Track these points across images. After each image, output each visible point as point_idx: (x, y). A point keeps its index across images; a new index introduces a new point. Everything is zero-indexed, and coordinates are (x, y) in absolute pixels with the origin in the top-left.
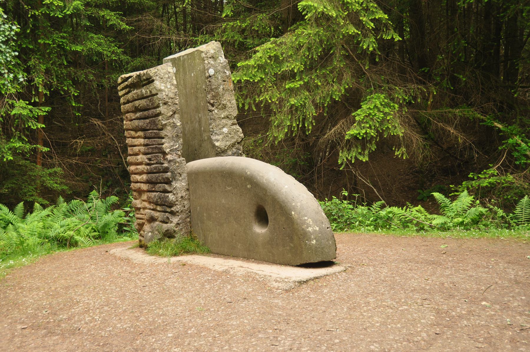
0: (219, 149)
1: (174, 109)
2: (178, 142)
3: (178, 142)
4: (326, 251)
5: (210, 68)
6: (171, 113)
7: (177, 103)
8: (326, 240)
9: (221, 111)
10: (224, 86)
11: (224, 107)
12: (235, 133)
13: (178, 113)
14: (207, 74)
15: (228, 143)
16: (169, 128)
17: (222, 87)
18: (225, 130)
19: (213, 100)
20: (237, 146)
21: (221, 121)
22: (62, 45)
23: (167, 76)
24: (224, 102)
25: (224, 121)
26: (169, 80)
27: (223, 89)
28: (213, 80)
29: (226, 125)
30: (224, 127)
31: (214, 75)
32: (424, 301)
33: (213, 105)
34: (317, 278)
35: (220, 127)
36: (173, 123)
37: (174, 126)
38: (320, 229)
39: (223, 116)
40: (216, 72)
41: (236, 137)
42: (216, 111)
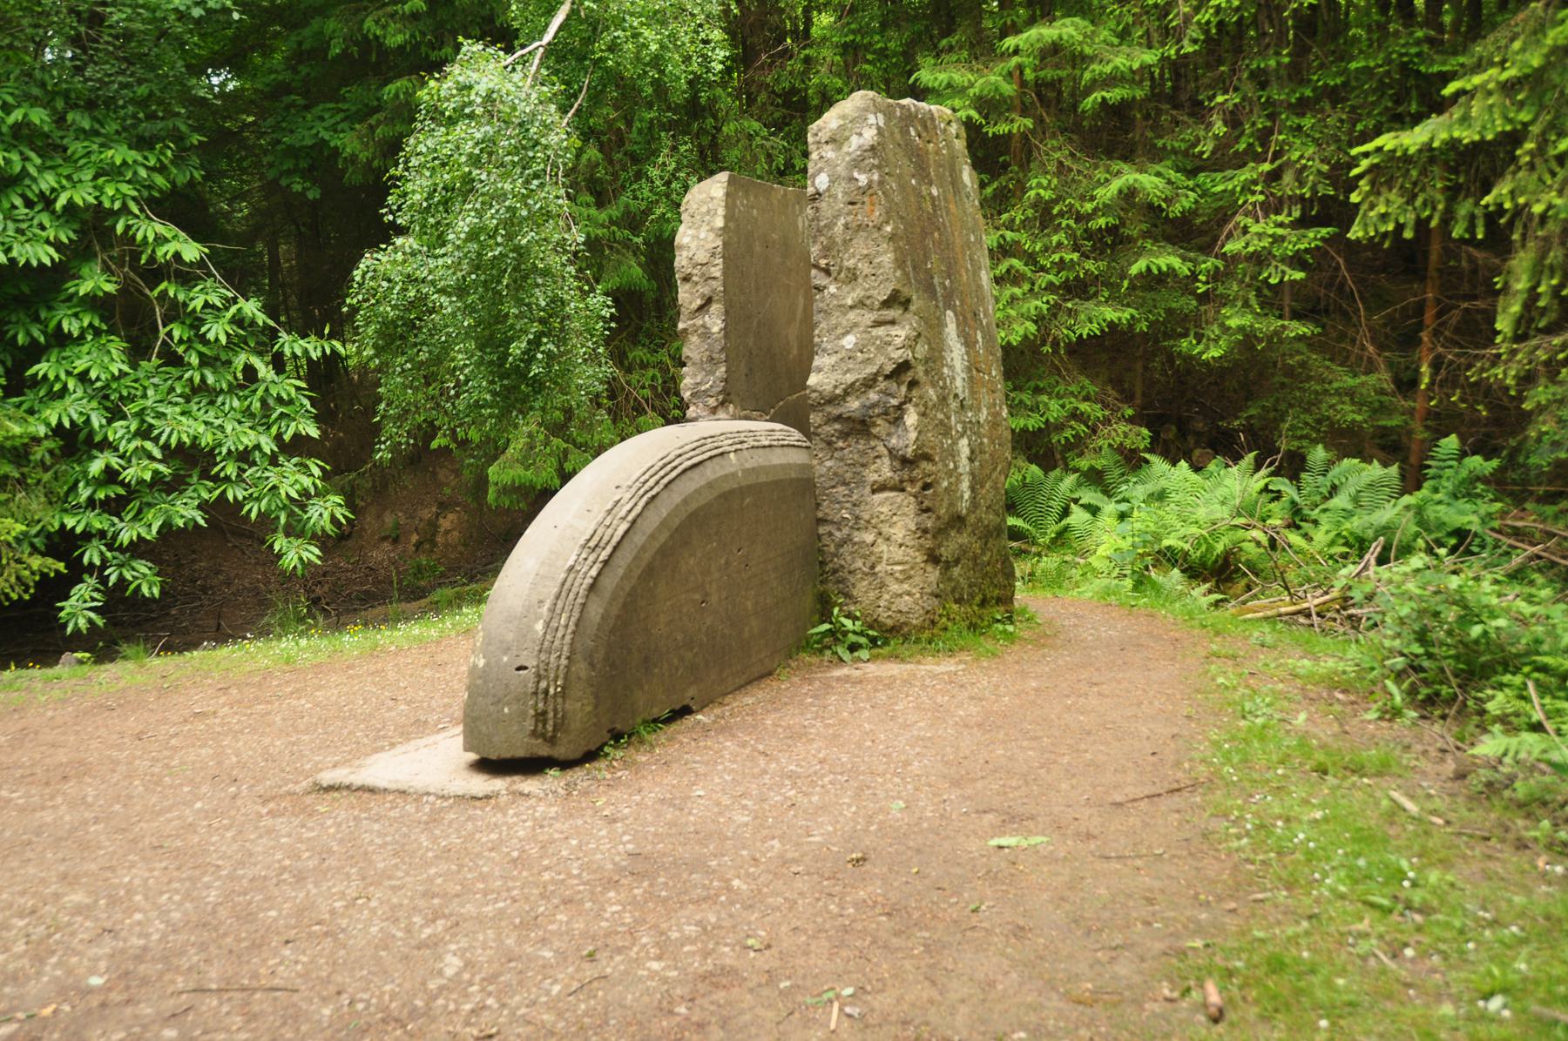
0: (814, 395)
1: (706, 290)
2: (713, 373)
3: (713, 373)
4: (484, 729)
5: (820, 170)
6: (699, 302)
7: (718, 274)
8: (490, 700)
9: (846, 289)
10: (849, 219)
11: (853, 277)
12: (878, 348)
13: (718, 301)
14: (810, 190)
15: (850, 378)
16: (694, 339)
17: (842, 221)
18: (849, 341)
19: (825, 257)
20: (882, 385)
21: (845, 314)
22: (1411, 61)
23: (704, 209)
24: (850, 263)
25: (852, 315)
26: (707, 218)
27: (846, 226)
28: (823, 205)
29: (856, 325)
30: (848, 332)
31: (828, 189)
32: (1257, 906)
33: (827, 272)
34: (372, 790)
35: (840, 331)
36: (704, 326)
37: (706, 334)
38: (487, 664)
39: (850, 302)
40: (833, 180)
41: (881, 360)
42: (832, 289)
